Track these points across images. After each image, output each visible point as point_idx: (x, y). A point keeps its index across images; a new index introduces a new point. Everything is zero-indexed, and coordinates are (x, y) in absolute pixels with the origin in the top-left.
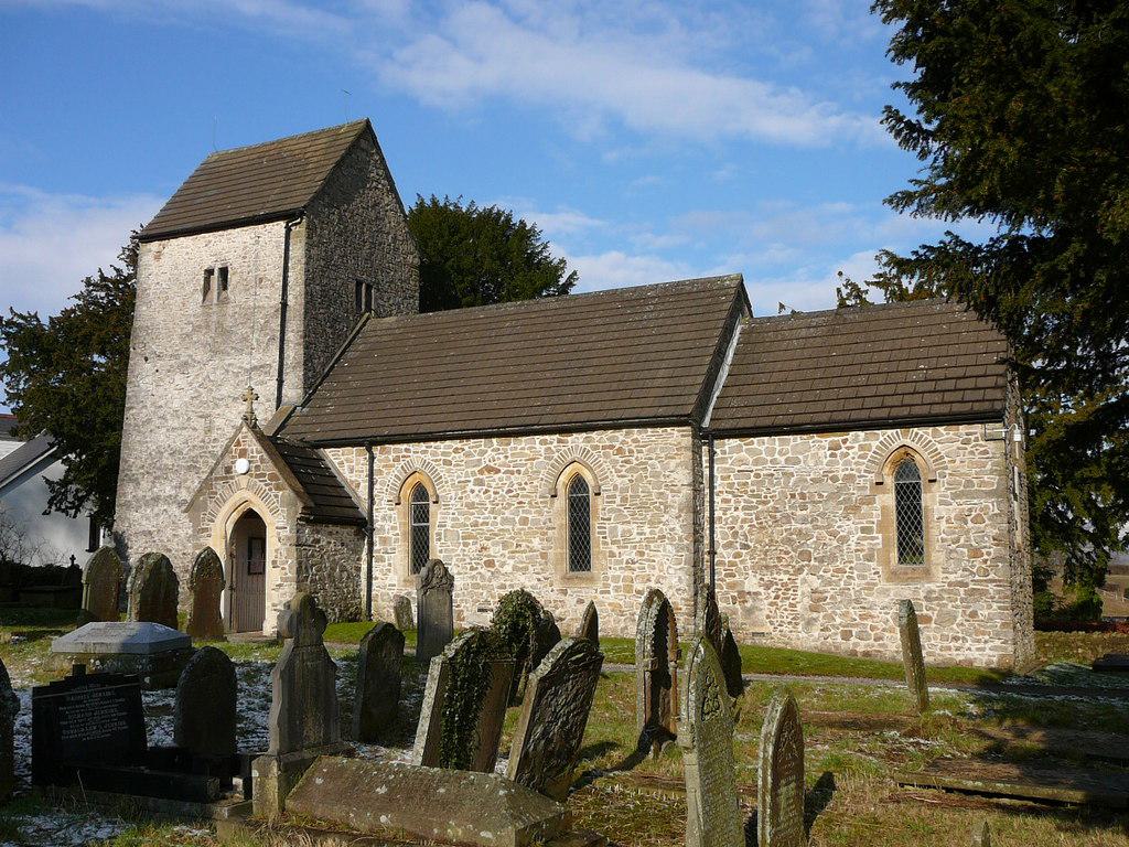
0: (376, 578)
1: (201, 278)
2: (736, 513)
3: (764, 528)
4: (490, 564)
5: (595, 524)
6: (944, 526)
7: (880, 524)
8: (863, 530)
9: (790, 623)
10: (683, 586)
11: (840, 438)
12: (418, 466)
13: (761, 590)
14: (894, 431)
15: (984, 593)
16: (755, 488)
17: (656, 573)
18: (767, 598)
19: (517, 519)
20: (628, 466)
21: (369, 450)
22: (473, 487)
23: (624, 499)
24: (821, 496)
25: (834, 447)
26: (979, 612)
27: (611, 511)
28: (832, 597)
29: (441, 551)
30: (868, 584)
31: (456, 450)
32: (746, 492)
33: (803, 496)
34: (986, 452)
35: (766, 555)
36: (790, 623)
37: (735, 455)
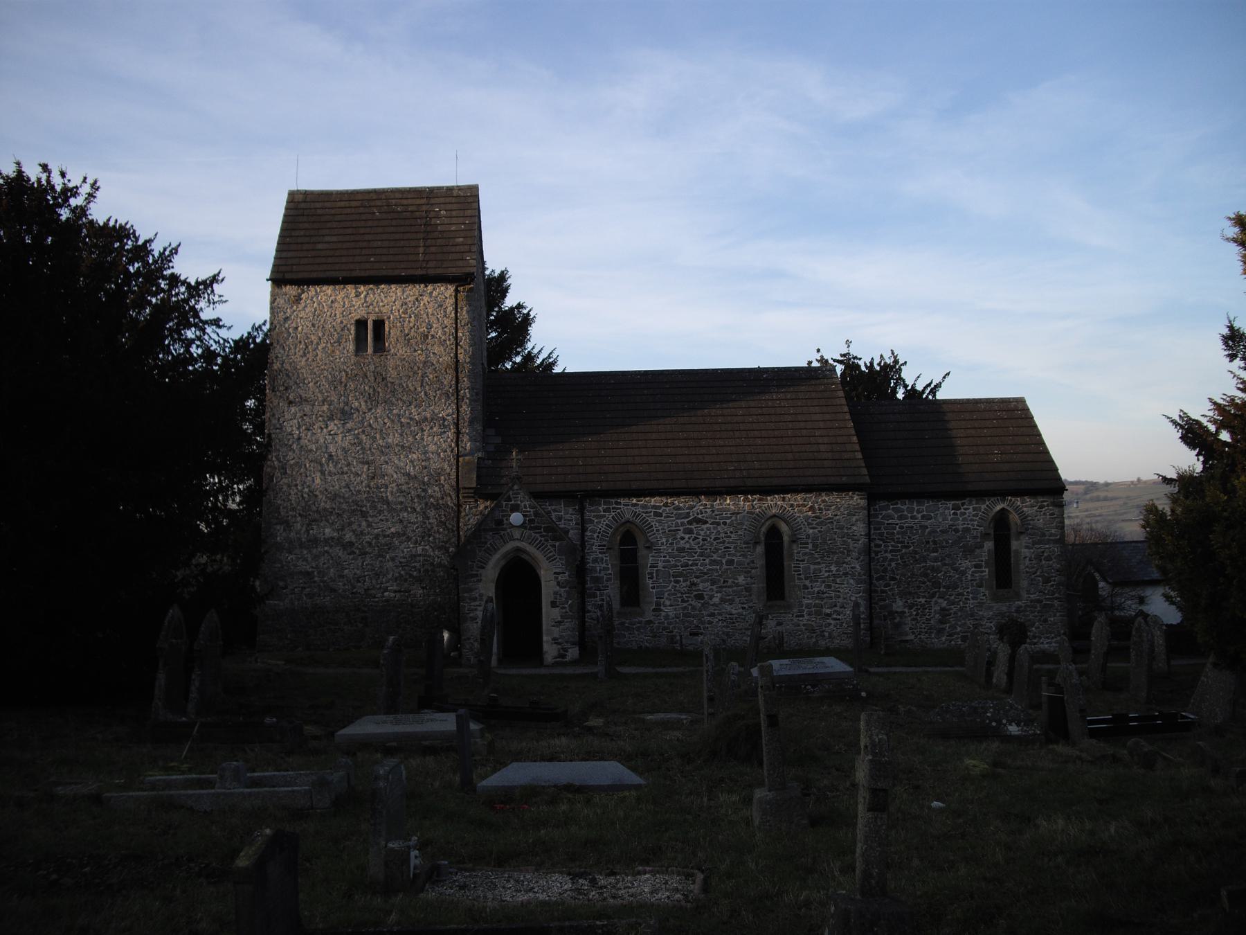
0: (589, 612)
3: (908, 565)
4: (699, 597)
6: (1027, 562)
8: (976, 566)
9: (926, 633)
11: (960, 502)
12: (628, 516)
13: (906, 610)
14: (996, 498)
15: (1052, 606)
16: (900, 536)
17: (841, 600)
18: (910, 616)
19: (724, 562)
20: (818, 520)
21: (582, 511)
22: (683, 535)
23: (815, 546)
24: (947, 542)
25: (956, 508)
26: (1049, 619)
27: (805, 554)
28: (955, 613)
29: (653, 588)
30: (979, 603)
31: (666, 505)
32: (893, 540)
33: (935, 542)
34: (1053, 514)
35: (908, 584)
36: (926, 633)
37: (884, 512)
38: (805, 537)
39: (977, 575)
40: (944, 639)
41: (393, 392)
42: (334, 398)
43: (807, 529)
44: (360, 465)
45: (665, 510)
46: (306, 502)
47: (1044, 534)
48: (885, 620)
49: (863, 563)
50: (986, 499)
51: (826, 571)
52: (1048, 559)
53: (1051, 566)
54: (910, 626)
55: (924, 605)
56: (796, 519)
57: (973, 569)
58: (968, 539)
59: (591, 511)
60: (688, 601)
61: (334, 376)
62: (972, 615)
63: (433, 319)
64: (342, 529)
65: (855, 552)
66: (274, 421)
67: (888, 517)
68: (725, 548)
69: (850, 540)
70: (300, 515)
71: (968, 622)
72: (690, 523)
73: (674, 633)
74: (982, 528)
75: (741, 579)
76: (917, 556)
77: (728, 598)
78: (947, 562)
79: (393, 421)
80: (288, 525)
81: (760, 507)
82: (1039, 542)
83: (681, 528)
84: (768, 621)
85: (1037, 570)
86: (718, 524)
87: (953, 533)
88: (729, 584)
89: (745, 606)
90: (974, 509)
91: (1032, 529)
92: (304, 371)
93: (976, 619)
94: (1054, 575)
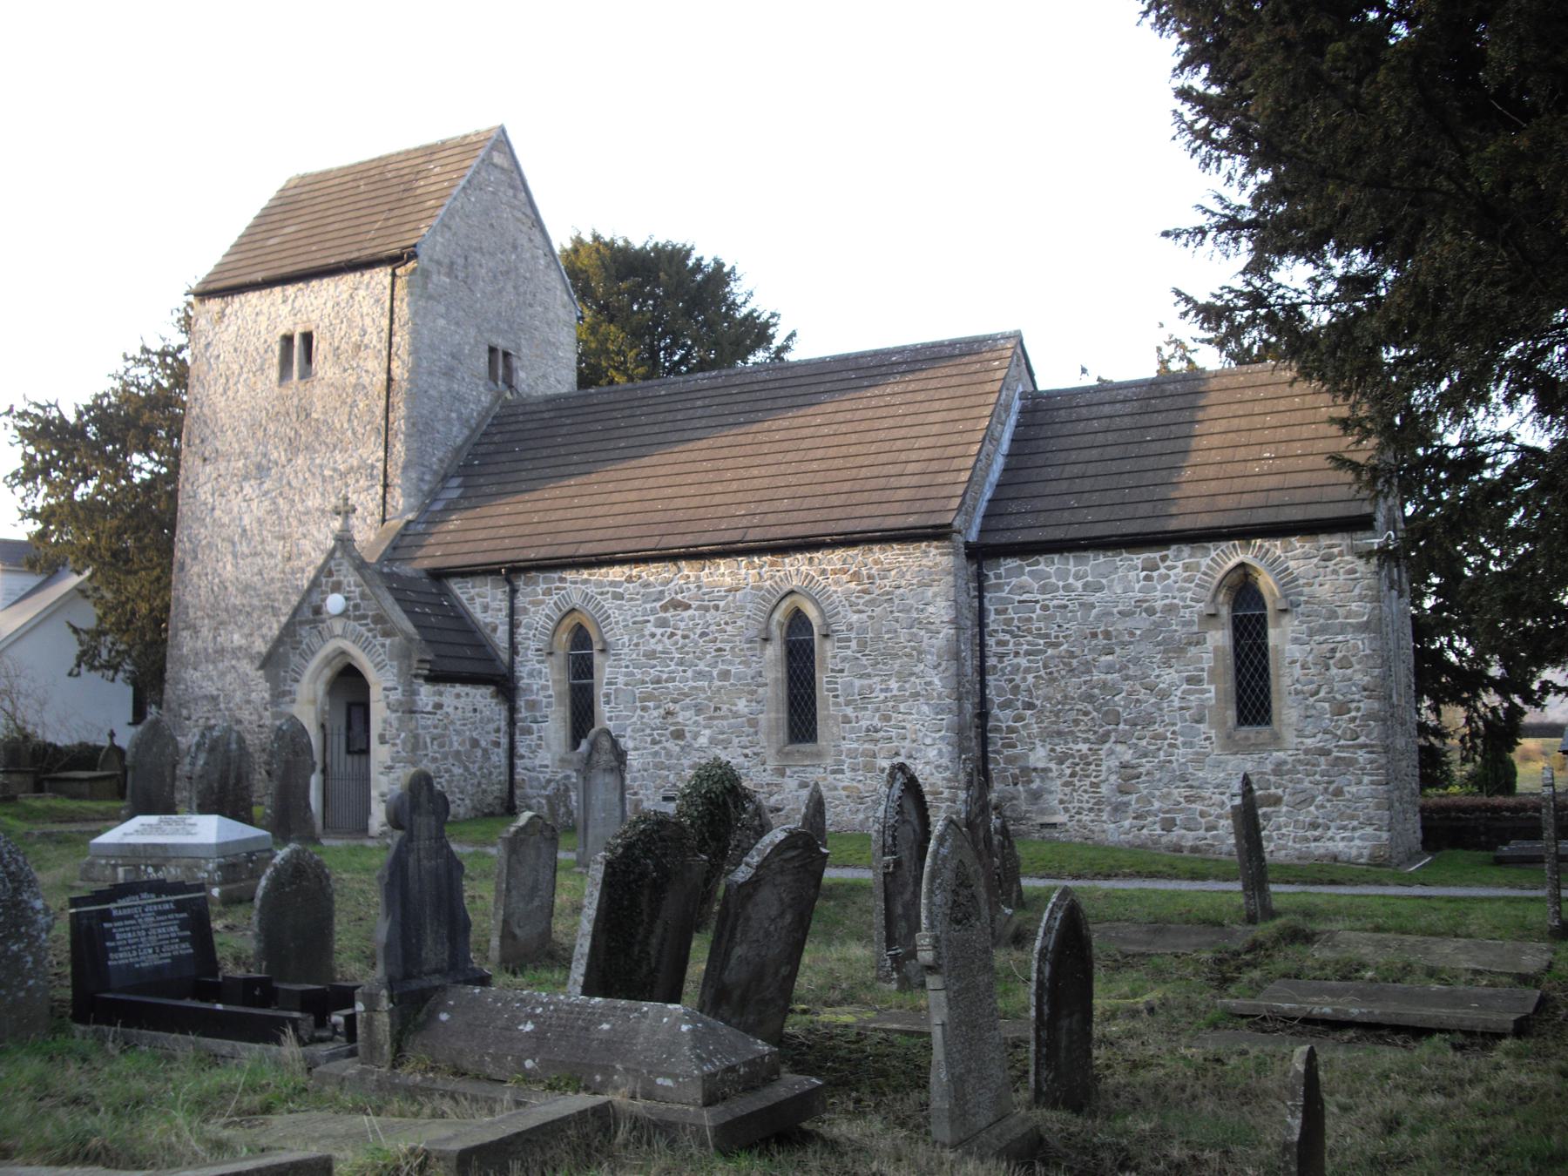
0: (522, 757)
1: (277, 348)
2: (1015, 661)
3: (1055, 680)
4: (678, 735)
5: (822, 678)
6: (1297, 671)
7: (1212, 671)
8: (1189, 680)
9: (1091, 810)
10: (945, 761)
11: (1157, 555)
12: (576, 600)
13: (1053, 765)
17: (907, 743)
19: (715, 673)
20: (867, 597)
22: (654, 630)
23: (863, 644)
24: (1132, 634)
25: (1151, 567)
27: (844, 659)
29: (610, 719)
31: (629, 580)
33: (1107, 635)
36: (1091, 810)
37: (1014, 581)
38: (844, 628)
39: (1192, 698)
40: (1127, 823)
41: (317, 433)
42: (251, 449)
43: (850, 614)
44: (275, 542)
45: (628, 588)
46: (216, 597)
47: (1335, 612)
48: (1016, 784)
49: (946, 674)
50: (1210, 545)
51: (882, 690)
52: (1345, 664)
53: (1350, 680)
54: (1060, 796)
55: (1086, 756)
56: (831, 596)
57: (1185, 686)
58: (1174, 627)
59: (525, 595)
60: (660, 742)
61: (253, 419)
62: (1183, 778)
63: (368, 321)
64: (251, 635)
65: (932, 654)
66: (188, 487)
67: (1021, 587)
68: (716, 650)
69: (922, 633)
70: (208, 616)
71: (1176, 792)
72: (665, 608)
73: (640, 797)
74: (1202, 604)
75: (742, 705)
76: (1075, 662)
77: (721, 737)
78: (1131, 673)
79: (313, 474)
80: (196, 631)
81: (772, 577)
82: (1323, 630)
83: (652, 618)
84: (786, 779)
85: (1320, 686)
86: (707, 609)
87: (1144, 614)
88: (722, 713)
89: (747, 751)
90: (1187, 568)
91: (1306, 602)
92: (222, 414)
93: (1191, 787)
94: (1357, 697)
